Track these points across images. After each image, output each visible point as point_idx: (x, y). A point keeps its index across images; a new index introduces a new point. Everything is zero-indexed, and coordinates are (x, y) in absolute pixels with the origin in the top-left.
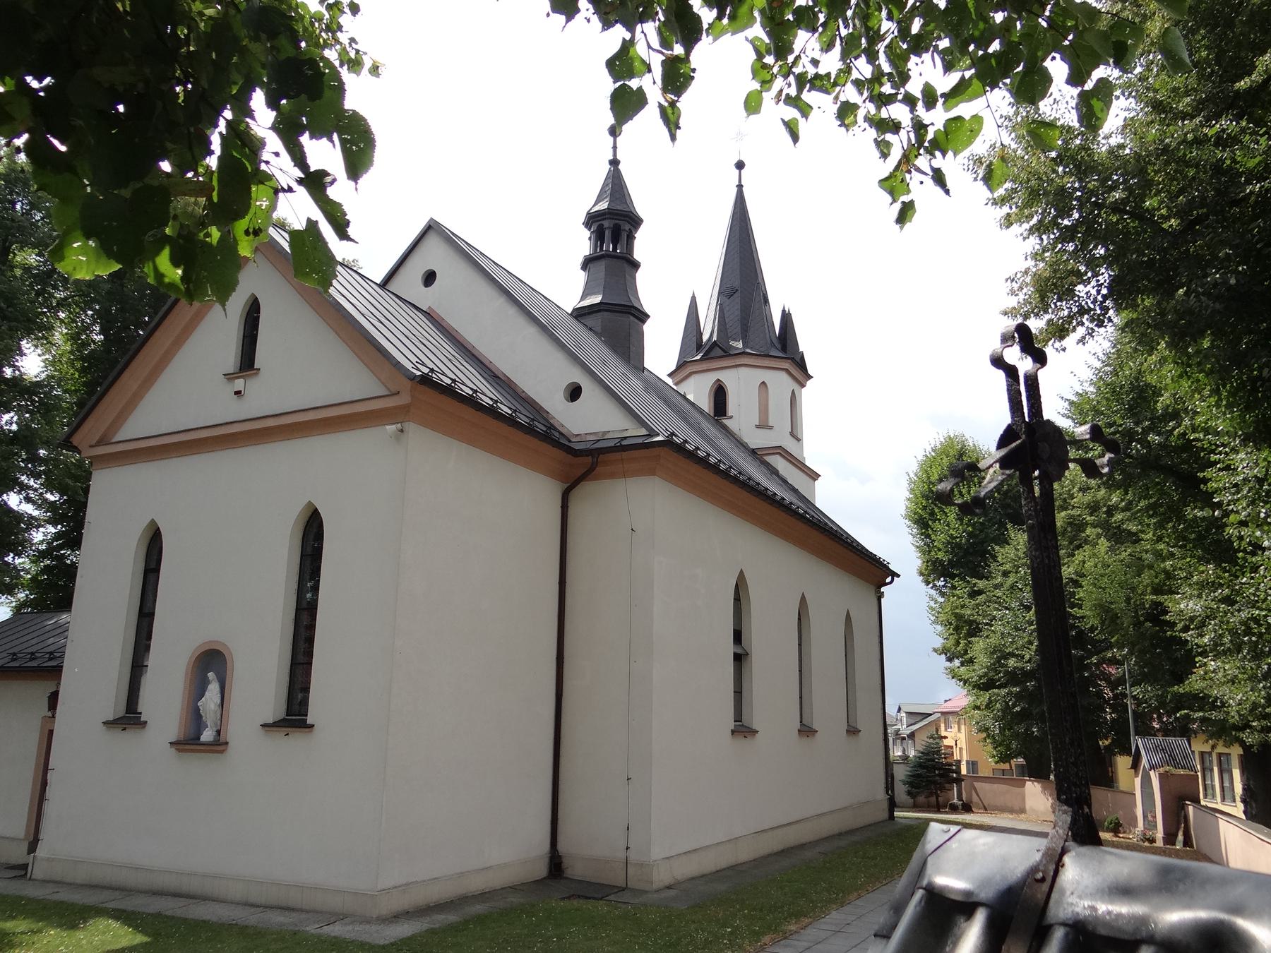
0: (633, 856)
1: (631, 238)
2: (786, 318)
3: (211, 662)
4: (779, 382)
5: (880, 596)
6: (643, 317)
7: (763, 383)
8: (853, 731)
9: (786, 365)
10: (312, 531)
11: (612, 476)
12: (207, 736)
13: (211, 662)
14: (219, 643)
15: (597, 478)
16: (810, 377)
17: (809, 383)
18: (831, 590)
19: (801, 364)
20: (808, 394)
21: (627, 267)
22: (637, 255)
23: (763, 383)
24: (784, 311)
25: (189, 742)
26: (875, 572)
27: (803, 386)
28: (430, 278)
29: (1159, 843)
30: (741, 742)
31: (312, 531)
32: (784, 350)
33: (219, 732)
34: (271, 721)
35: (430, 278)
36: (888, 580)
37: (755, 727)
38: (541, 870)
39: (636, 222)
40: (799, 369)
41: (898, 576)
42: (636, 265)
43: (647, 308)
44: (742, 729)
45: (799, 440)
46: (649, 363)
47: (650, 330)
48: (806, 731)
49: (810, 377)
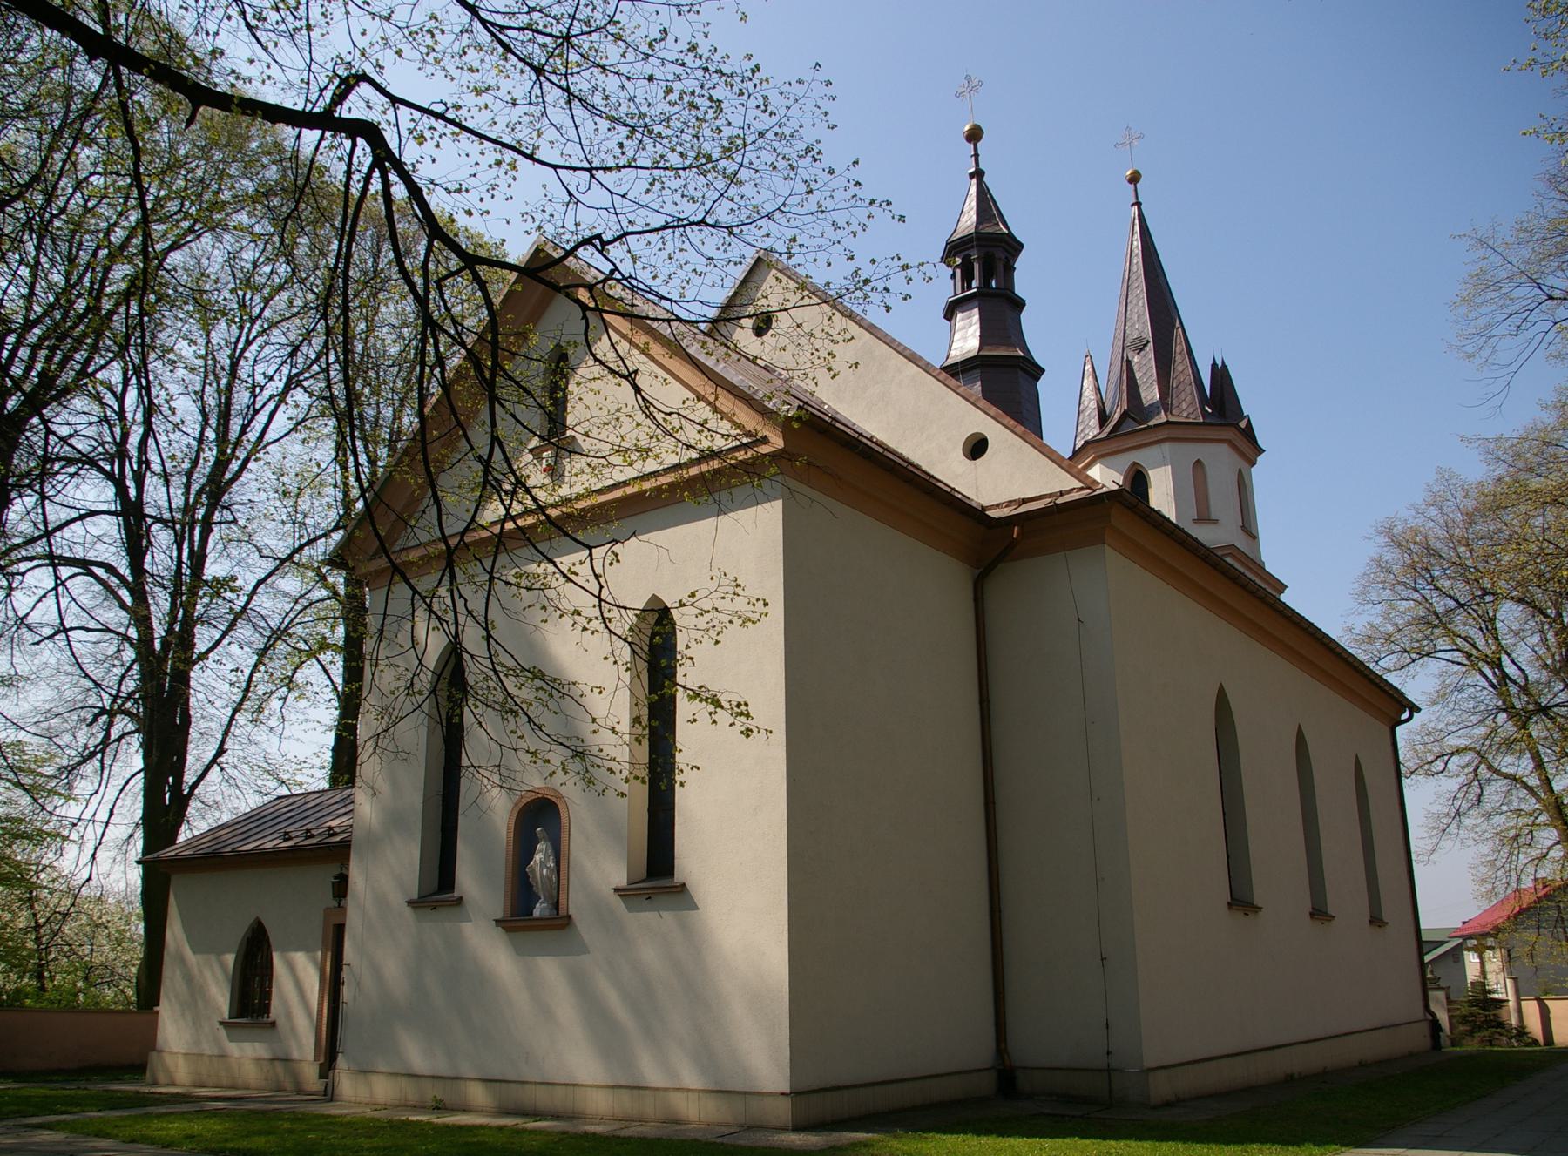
1: (1009, 269)
2: (1221, 374)
3: (539, 817)
4: (1219, 458)
6: (1036, 372)
7: (1198, 461)
8: (1376, 920)
12: (539, 910)
13: (539, 817)
14: (561, 797)
16: (1261, 451)
18: (1335, 724)
20: (1259, 474)
23: (1198, 461)
24: (1214, 365)
29: (1427, 958)
32: (1221, 408)
33: (556, 906)
36: (1405, 716)
39: (1013, 247)
40: (1248, 445)
41: (1419, 710)
42: (1019, 304)
43: (1039, 359)
45: (1254, 537)
46: (1048, 439)
47: (1045, 387)
49: (1261, 451)
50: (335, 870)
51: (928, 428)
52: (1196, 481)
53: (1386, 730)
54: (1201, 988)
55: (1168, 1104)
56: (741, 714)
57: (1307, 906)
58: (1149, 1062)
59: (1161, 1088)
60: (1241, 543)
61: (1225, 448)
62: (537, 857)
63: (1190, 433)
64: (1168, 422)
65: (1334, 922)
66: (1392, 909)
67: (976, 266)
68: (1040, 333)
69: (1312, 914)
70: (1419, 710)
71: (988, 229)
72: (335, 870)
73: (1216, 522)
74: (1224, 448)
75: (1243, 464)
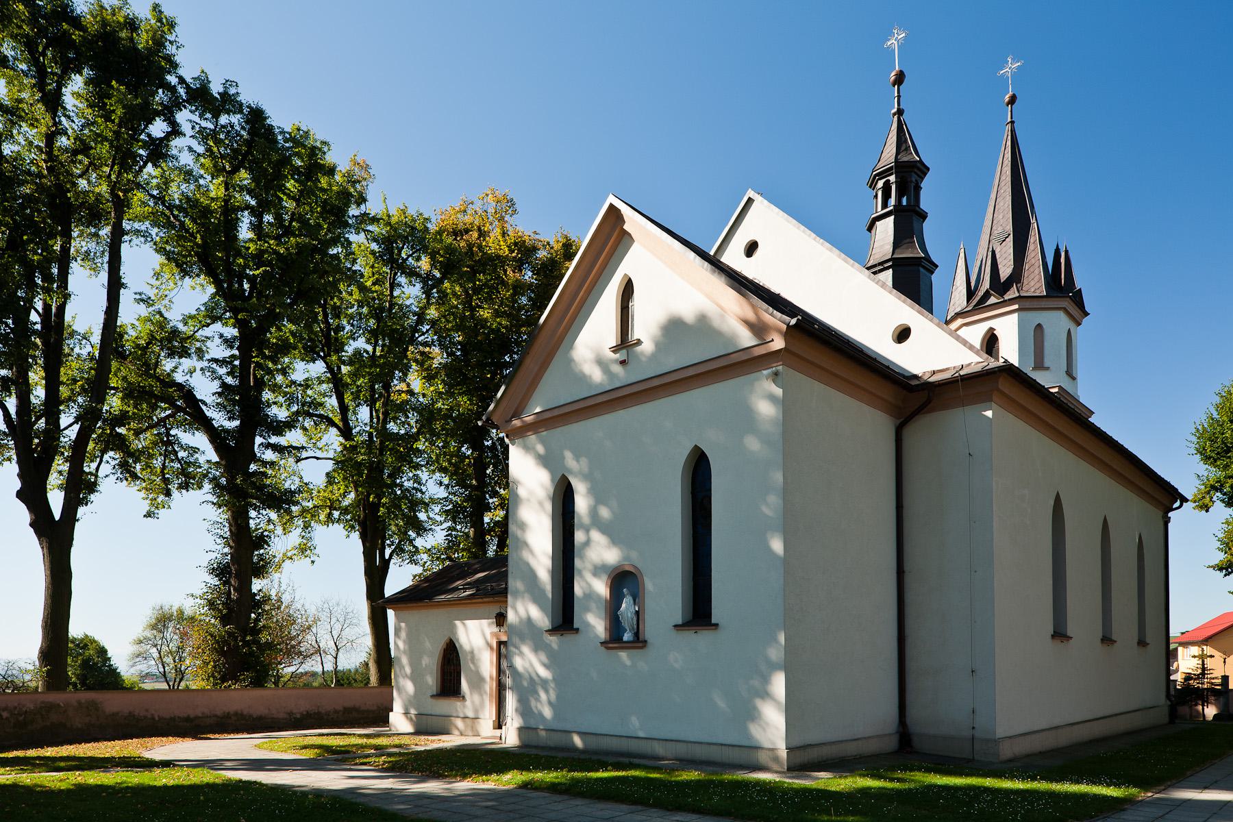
0: (978, 734)
1: (918, 188)
4: (1056, 322)
5: (1167, 521)
8: (1142, 643)
9: (1066, 303)
10: (699, 471)
11: (946, 407)
12: (627, 637)
13: (623, 580)
15: (933, 410)
16: (1087, 314)
17: (1085, 320)
18: (1129, 509)
19: (1078, 299)
21: (915, 218)
22: (924, 205)
25: (615, 638)
26: (1166, 497)
27: (1079, 324)
28: (751, 249)
30: (1057, 642)
31: (699, 471)
32: (1062, 288)
34: (680, 622)
35: (751, 249)
36: (1177, 504)
37: (1069, 634)
38: (892, 744)
44: (1060, 634)
45: (1074, 379)
48: (1107, 640)
49: (1087, 314)
50: (495, 609)
51: (862, 309)
52: (1035, 339)
53: (1160, 514)
54: (1026, 684)
55: (1010, 761)
56: (166, 481)
57: (1050, 630)
58: (998, 736)
59: (1007, 751)
60: (1067, 384)
61: (1061, 314)
62: (624, 605)
63: (1035, 304)
64: (1020, 297)
65: (1071, 641)
66: (1152, 636)
67: (894, 187)
68: (935, 237)
69: (1102, 640)
70: (1187, 500)
71: (904, 158)
72: (495, 609)
73: (1048, 368)
74: (1061, 315)
75: (1071, 325)
